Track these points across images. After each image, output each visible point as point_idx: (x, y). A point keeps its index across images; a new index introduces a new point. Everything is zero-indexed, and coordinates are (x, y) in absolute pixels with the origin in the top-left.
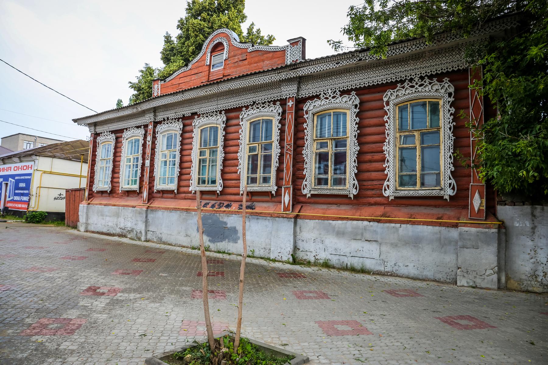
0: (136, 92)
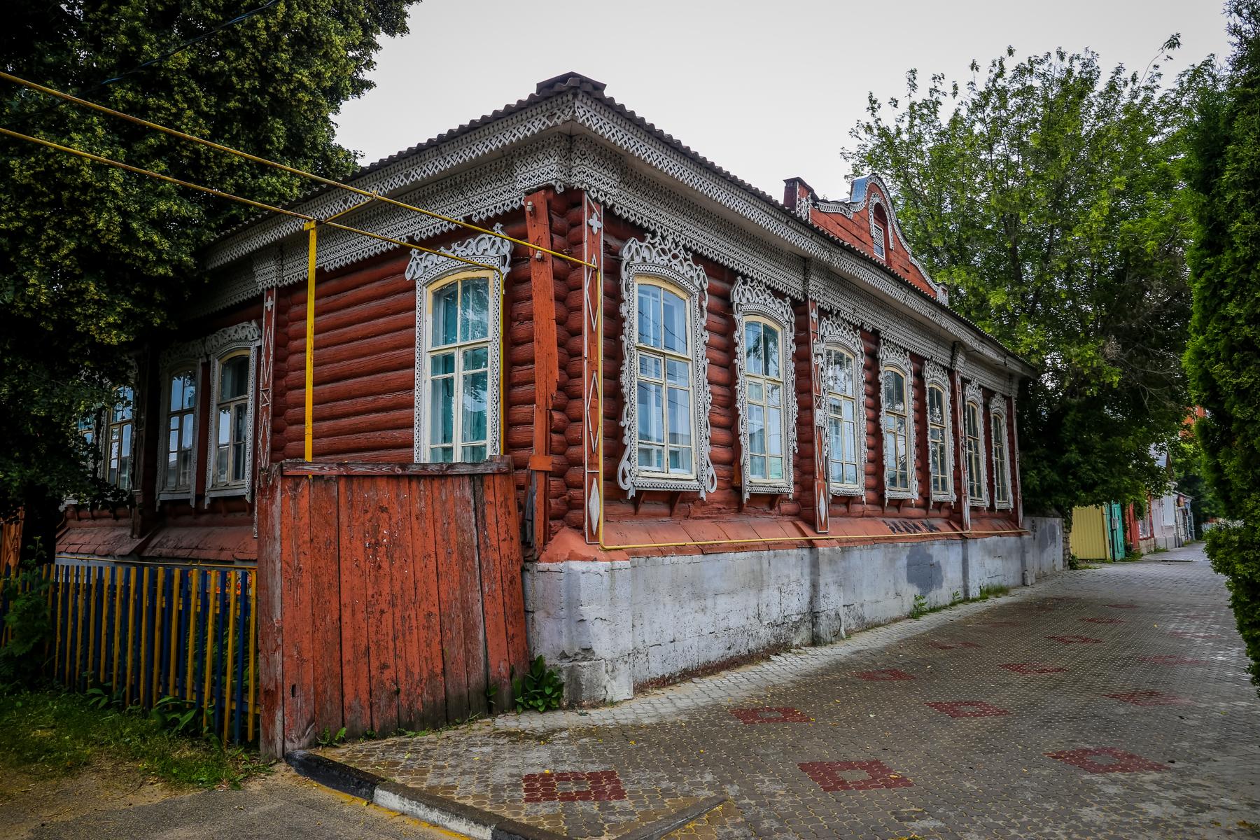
0: (331, 116)
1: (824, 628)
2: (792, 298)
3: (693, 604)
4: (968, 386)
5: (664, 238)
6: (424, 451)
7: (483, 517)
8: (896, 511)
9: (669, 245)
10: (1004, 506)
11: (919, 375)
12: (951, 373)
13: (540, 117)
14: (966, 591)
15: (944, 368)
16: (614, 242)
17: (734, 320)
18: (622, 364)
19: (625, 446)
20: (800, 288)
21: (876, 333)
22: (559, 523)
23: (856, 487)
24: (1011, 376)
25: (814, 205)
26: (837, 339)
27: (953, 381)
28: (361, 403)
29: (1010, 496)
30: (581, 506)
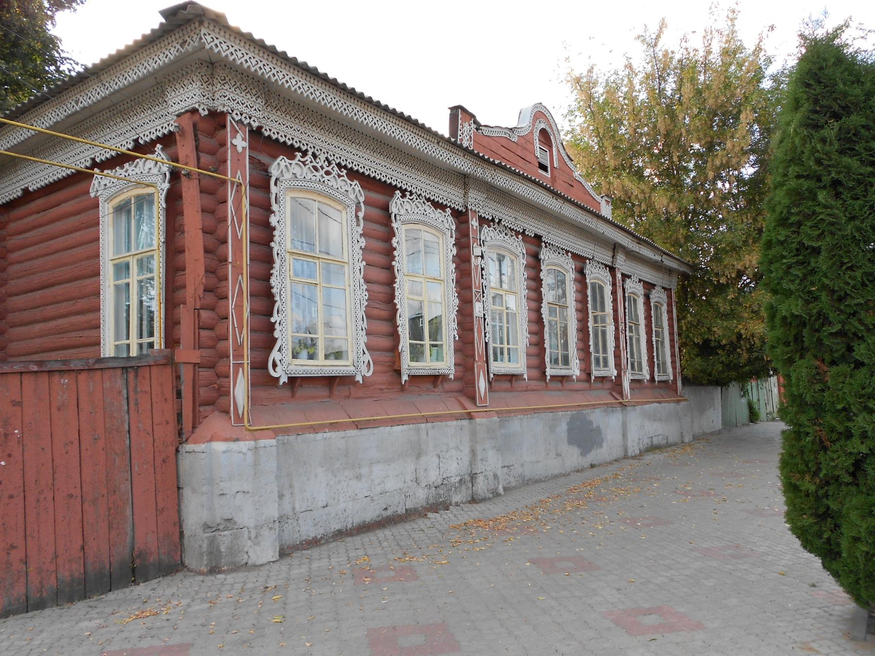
1: (482, 486)
2: (453, 209)
3: (347, 473)
4: (628, 281)
5: (314, 156)
6: (108, 350)
7: (137, 404)
8: (559, 385)
9: (321, 162)
10: (664, 378)
11: (581, 272)
12: (612, 270)
13: (175, 44)
14: (626, 450)
15: (606, 266)
16: (264, 159)
17: (392, 228)
18: (272, 268)
19: (277, 339)
20: (461, 201)
21: (538, 238)
22: (208, 408)
23: (518, 365)
24: (670, 271)
25: (477, 129)
26: (499, 243)
27: (614, 276)
28: (64, 307)
29: (670, 370)
30: (228, 393)
